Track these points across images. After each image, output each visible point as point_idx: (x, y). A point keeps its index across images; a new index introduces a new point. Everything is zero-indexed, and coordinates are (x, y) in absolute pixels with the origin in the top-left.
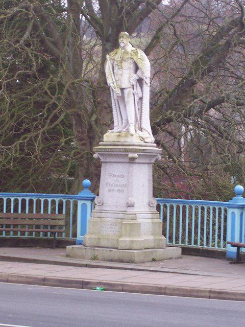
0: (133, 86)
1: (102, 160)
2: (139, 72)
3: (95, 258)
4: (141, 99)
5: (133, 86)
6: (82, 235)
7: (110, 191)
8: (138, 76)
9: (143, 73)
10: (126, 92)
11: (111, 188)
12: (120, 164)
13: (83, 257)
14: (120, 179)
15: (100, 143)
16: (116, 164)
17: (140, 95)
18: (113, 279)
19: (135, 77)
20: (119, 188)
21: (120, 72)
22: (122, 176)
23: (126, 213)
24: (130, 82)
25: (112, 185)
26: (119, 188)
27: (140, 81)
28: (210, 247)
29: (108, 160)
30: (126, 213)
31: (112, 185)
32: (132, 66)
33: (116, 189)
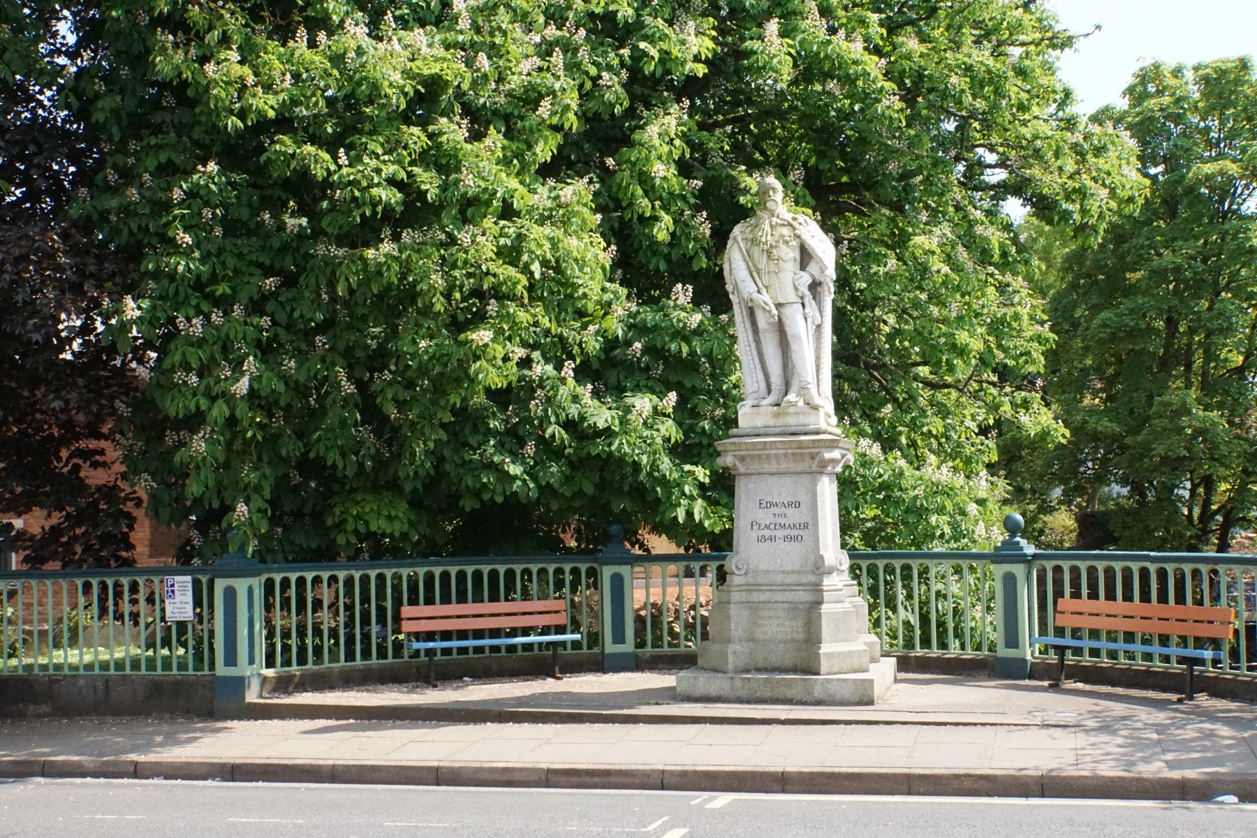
0: (802, 298)
1: (742, 469)
2: (813, 268)
3: (286, 635)
4: (819, 327)
5: (802, 298)
6: (226, 664)
7: (763, 539)
8: (812, 275)
9: (822, 270)
10: (787, 311)
11: (767, 533)
12: (785, 479)
13: (1232, 810)
14: (791, 511)
15: (734, 431)
16: (775, 478)
17: (818, 321)
18: (275, 754)
19: (805, 279)
20: (786, 532)
21: (772, 268)
22: (798, 505)
23: (755, 274)
24: (796, 289)
25: (767, 527)
26: (786, 532)
27: (815, 286)
28: (935, 652)
29: (756, 467)
30: (755, 274)
31: (767, 527)
32: (797, 254)
33: (780, 534)
